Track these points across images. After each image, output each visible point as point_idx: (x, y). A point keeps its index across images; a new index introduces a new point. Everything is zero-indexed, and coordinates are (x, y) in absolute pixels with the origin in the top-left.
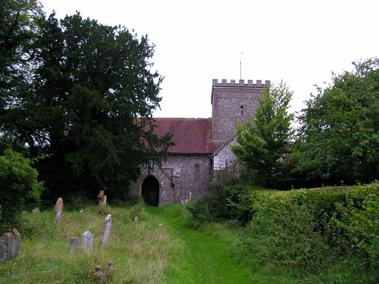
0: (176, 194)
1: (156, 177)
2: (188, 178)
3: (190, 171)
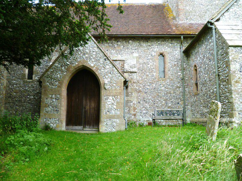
0: (131, 102)
1: (94, 69)
2: (147, 76)
3: (151, 64)
